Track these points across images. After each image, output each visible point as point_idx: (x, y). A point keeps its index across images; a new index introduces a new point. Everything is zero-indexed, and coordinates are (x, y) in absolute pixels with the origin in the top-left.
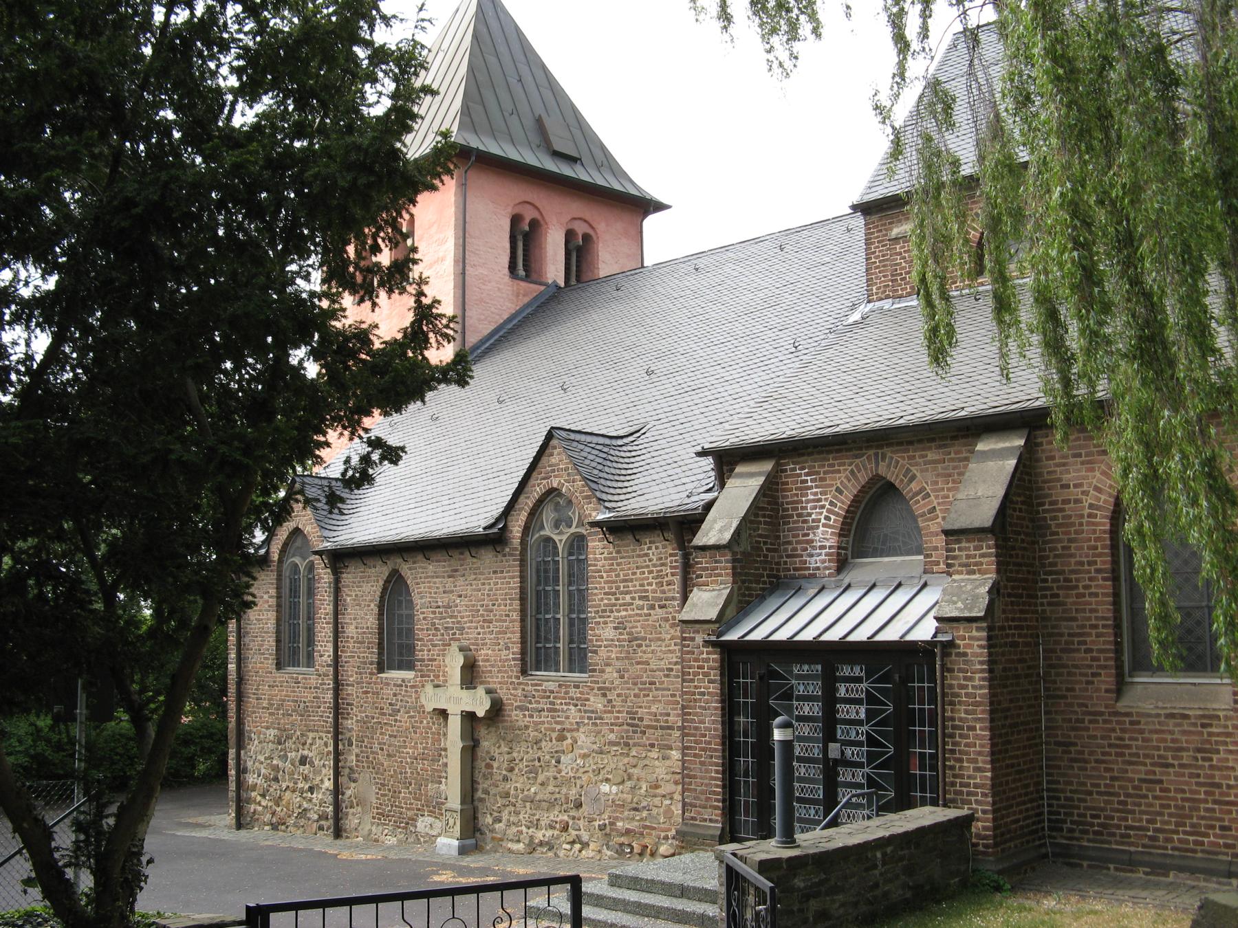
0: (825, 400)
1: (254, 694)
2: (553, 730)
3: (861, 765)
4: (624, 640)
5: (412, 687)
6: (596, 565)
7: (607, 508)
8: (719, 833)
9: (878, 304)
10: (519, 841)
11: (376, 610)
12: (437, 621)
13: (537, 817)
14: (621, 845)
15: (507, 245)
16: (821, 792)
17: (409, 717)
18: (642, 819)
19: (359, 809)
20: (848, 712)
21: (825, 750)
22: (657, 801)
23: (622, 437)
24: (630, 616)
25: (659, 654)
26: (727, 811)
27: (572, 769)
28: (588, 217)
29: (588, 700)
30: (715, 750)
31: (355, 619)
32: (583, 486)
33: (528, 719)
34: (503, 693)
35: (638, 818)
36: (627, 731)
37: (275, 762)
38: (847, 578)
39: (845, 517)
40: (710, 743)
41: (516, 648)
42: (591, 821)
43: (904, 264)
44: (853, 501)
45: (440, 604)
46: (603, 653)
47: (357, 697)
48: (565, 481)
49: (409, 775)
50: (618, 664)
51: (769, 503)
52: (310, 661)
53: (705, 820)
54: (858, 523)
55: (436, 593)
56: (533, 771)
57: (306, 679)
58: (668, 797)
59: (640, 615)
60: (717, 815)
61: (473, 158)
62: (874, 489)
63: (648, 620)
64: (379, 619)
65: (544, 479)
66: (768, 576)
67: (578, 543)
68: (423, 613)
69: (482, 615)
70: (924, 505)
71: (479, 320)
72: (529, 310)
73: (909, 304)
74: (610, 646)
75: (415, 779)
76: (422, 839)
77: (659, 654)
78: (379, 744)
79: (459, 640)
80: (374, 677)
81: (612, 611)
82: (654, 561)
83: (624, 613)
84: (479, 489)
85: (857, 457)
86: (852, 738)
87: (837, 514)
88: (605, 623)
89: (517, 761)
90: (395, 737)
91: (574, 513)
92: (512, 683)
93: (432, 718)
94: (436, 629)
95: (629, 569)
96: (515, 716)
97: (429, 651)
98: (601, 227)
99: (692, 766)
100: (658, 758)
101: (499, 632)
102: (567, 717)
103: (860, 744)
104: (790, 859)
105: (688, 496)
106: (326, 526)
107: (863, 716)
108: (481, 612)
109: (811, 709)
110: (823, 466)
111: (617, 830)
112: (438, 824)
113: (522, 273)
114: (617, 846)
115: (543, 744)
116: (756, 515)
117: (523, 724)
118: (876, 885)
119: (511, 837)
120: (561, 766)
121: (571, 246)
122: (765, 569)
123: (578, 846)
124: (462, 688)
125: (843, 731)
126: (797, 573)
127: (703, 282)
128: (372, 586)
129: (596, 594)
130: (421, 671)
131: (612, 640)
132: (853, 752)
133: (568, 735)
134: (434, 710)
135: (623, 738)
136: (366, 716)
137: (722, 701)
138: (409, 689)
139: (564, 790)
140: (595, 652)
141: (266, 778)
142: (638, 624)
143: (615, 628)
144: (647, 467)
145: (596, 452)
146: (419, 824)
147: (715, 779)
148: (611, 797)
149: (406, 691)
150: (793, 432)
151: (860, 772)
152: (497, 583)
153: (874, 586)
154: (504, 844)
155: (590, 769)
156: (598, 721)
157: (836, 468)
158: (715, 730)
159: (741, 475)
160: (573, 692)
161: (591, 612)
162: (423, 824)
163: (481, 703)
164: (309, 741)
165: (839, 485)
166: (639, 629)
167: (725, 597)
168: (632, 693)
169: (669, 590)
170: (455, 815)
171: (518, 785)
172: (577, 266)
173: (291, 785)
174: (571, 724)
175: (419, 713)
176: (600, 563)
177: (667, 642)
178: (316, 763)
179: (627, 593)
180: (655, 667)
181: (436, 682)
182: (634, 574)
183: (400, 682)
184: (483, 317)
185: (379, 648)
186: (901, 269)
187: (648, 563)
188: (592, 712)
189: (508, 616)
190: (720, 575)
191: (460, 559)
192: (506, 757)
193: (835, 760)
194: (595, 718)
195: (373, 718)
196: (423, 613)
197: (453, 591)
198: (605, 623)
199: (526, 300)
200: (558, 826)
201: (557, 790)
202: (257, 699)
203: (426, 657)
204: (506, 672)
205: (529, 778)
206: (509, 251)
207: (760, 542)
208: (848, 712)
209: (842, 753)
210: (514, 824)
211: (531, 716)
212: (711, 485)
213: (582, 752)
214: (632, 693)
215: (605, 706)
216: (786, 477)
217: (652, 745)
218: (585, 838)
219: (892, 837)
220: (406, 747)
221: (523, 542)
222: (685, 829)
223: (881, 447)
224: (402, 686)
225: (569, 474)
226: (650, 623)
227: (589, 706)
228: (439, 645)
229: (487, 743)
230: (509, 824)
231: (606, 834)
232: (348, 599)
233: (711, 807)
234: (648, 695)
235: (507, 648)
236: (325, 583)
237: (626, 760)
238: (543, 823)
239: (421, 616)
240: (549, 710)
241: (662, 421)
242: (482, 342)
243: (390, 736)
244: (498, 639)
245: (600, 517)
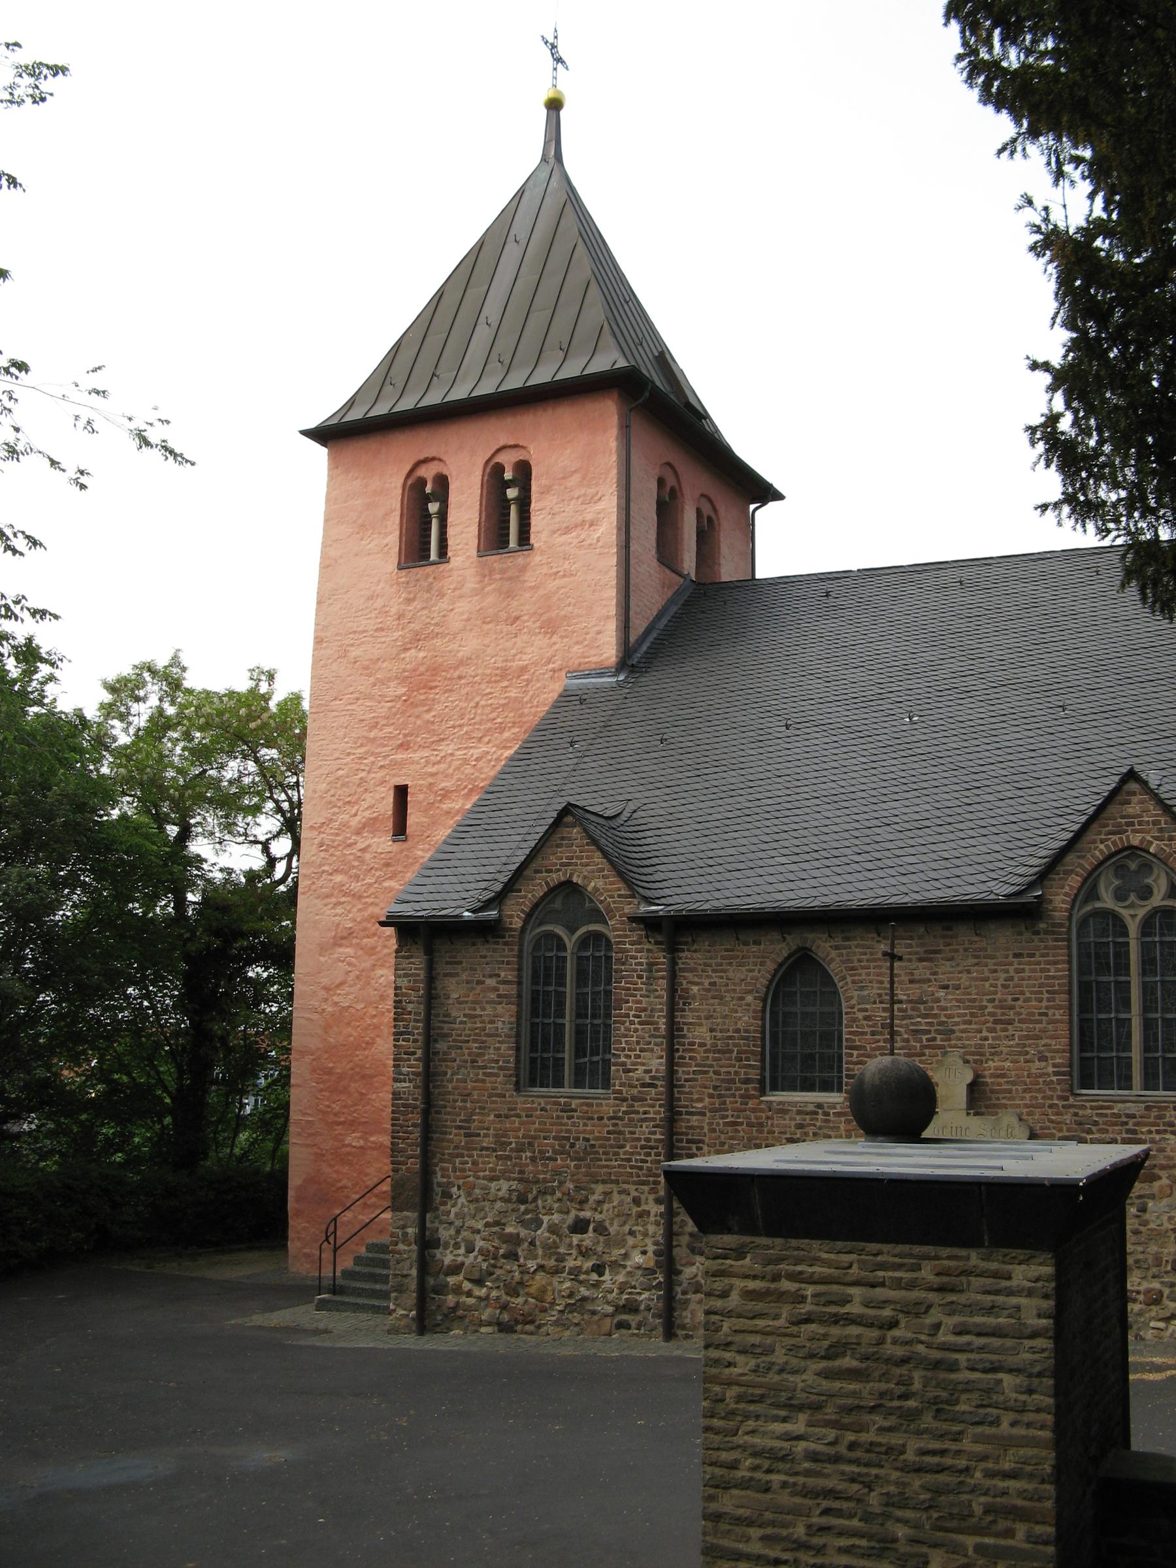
124: (968, 1114)
225: (1161, 830)
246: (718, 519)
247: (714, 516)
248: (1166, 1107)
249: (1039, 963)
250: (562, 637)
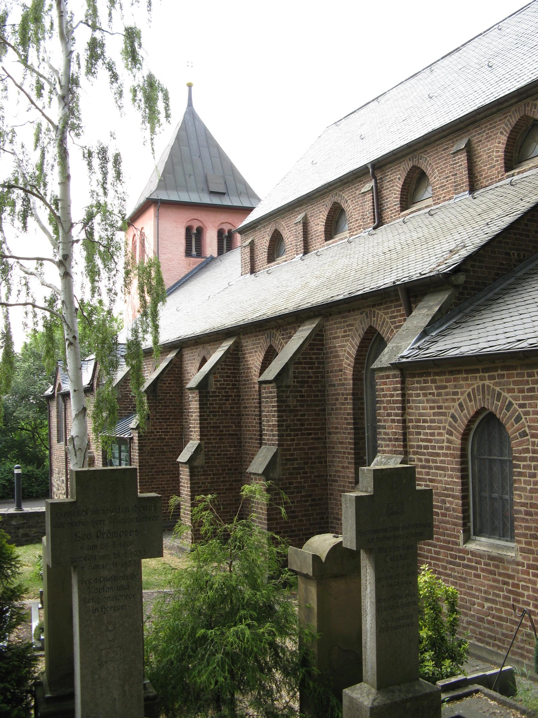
28: (230, 221)
113: (194, 253)
199: (194, 266)
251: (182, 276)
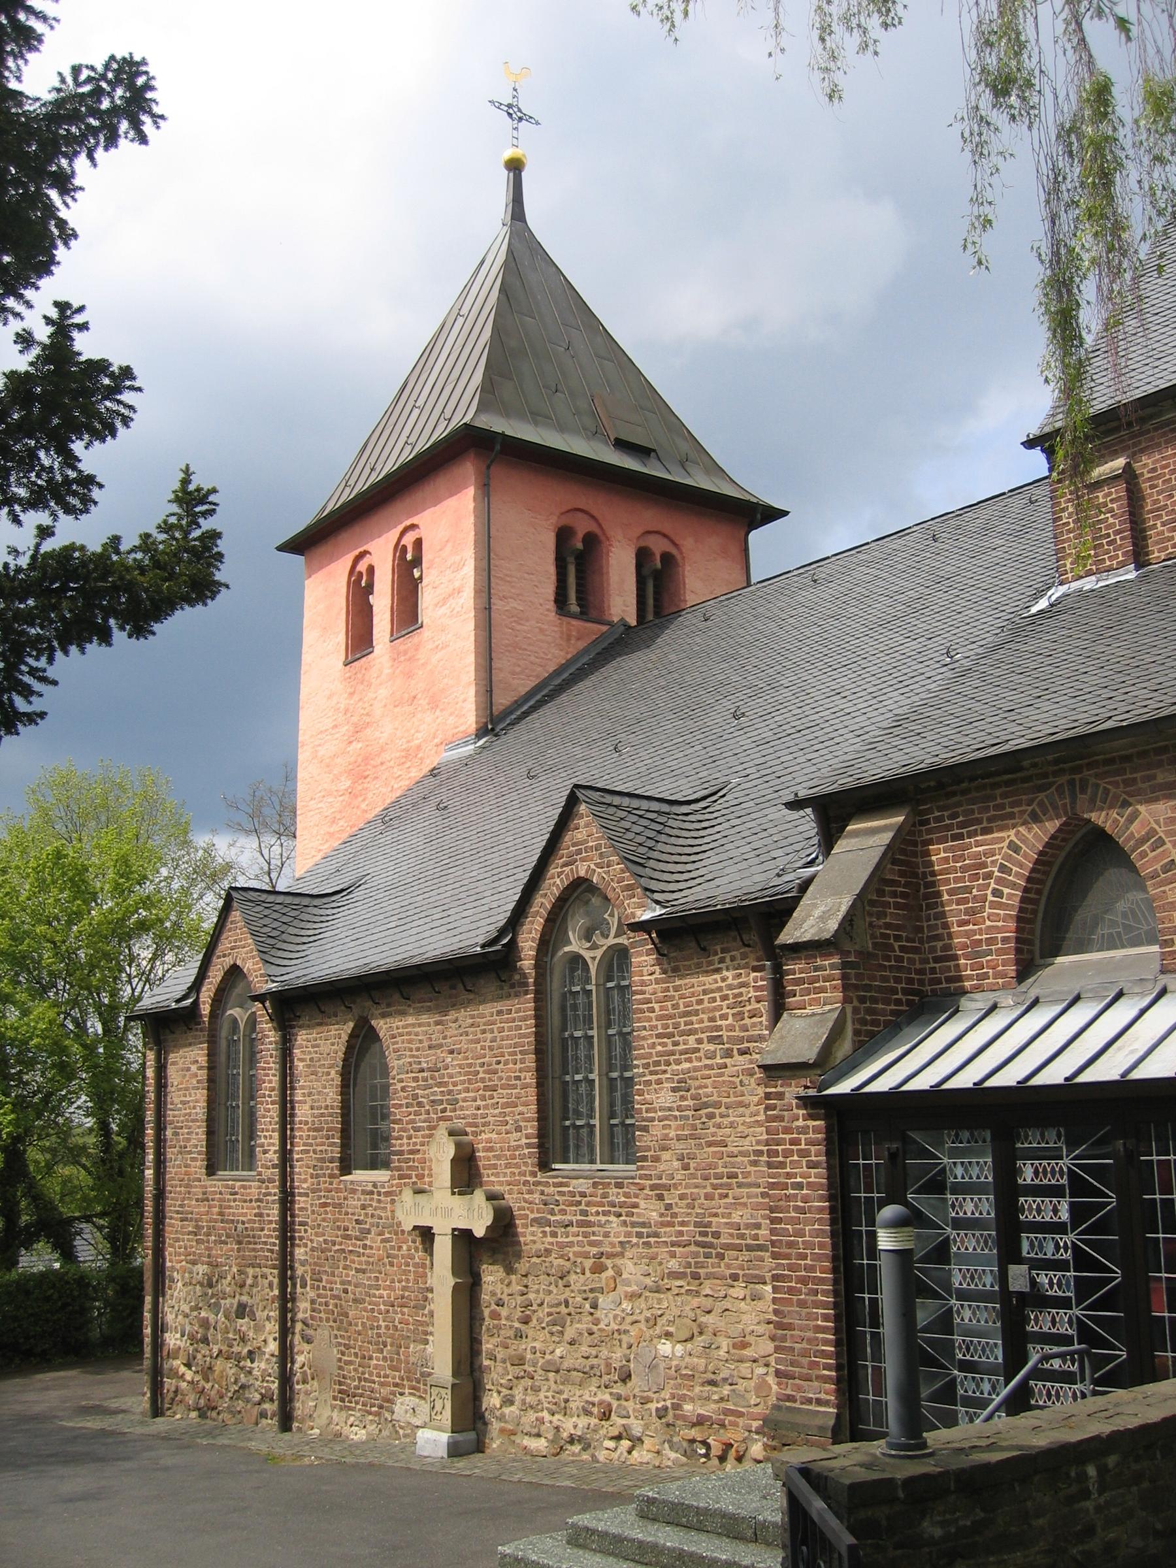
0: (988, 711)
1: (178, 1212)
2: (586, 1256)
3: (1065, 1303)
4: (688, 1108)
5: (387, 1194)
6: (643, 993)
7: (657, 902)
8: (832, 1422)
9: (1075, 585)
10: (539, 1435)
11: (338, 1080)
12: (420, 1092)
13: (565, 1396)
14: (692, 1441)
15: (552, 569)
16: (999, 1352)
17: (383, 1241)
18: (722, 1399)
19: (315, 1383)
20: (1039, 1210)
21: (1003, 1278)
22: (745, 1368)
23: (689, 803)
24: (696, 1069)
25: (741, 1128)
26: (845, 1385)
27: (615, 1317)
28: (666, 527)
29: (636, 1206)
30: (822, 1281)
31: (310, 1094)
32: (623, 871)
33: (549, 1239)
34: (512, 1200)
35: (716, 1397)
36: (696, 1255)
37: (203, 1314)
38: (1035, 986)
39: (1026, 890)
40: (811, 1268)
41: (531, 1128)
42: (645, 1401)
43: (1111, 520)
44: (1037, 862)
45: (424, 1065)
46: (656, 1130)
47: (313, 1212)
48: (597, 865)
49: (383, 1330)
50: (680, 1146)
51: (902, 874)
52: (250, 1161)
53: (809, 1401)
54: (1049, 898)
55: (418, 1049)
56: (558, 1322)
57: (244, 1187)
58: (762, 1361)
59: (710, 1067)
60: (828, 1390)
61: (498, 447)
62: (1071, 844)
63: (722, 1075)
64: (342, 1094)
65: (566, 865)
66: (906, 992)
67: (618, 959)
68: (401, 1081)
69: (483, 1080)
70: (1156, 859)
71: (513, 673)
72: (585, 660)
73: (1122, 578)
74: (666, 1118)
75: (392, 1337)
76: (401, 1432)
77: (741, 1128)
78: (342, 1283)
79: (450, 1119)
80: (336, 1181)
81: (668, 1064)
82: (730, 981)
83: (686, 1065)
84: (485, 894)
85: (1041, 789)
86: (1049, 1256)
87: (1013, 886)
88: (659, 1082)
89: (535, 1307)
90: (364, 1271)
91: (612, 915)
92: (526, 1183)
93: (414, 1242)
94: (420, 1104)
95: (693, 995)
96: (529, 1235)
97: (410, 1138)
98: (688, 543)
99: (786, 1309)
100: (744, 1299)
101: (507, 1105)
102: (606, 1235)
103: (1061, 1265)
104: (910, 1482)
105: (778, 875)
106: (272, 960)
107: (1064, 1215)
108: (481, 1075)
109: (976, 1206)
110: (987, 809)
111: (684, 1418)
112: (424, 1407)
113: (575, 608)
114: (685, 1444)
115: (572, 1278)
116: (880, 893)
117: (542, 1247)
118: (1090, 1531)
119: (527, 1429)
120: (599, 1314)
121: (646, 571)
122: (898, 980)
123: (626, 1443)
124: (453, 1193)
125: (1032, 1245)
126: (952, 985)
127: (823, 595)
128: (333, 1044)
129: (644, 1038)
130: (399, 1169)
131: (670, 1109)
132: (1051, 1280)
133: (609, 1263)
134: (415, 1228)
135: (689, 1265)
136: (325, 1241)
137: (831, 1198)
138: (382, 1198)
139: (604, 1353)
140: (645, 1129)
141: (192, 1337)
142: (708, 1081)
143: (674, 1090)
144: (724, 841)
145: (646, 823)
146: (397, 1408)
147: (824, 1330)
148: (674, 1363)
149: (379, 1201)
150: (936, 759)
151: (1063, 1315)
152: (501, 1030)
153: (1077, 999)
154: (517, 1439)
155: (641, 1318)
156: (652, 1240)
157: (1008, 810)
158: (821, 1246)
159: (856, 834)
160: (616, 1196)
161: (637, 1066)
162: (404, 1406)
163: (481, 1216)
164: (249, 1281)
165: (1013, 838)
166: (710, 1090)
167: (830, 1024)
168: (702, 1192)
169: (754, 1025)
170: (443, 1391)
171: (537, 1345)
172: (655, 600)
173: (224, 1348)
174: (613, 1245)
175: (396, 1234)
176: (649, 989)
177: (753, 1108)
178: (258, 1314)
179: (690, 1033)
180: (735, 1150)
181: (419, 1185)
182: (700, 1002)
183: (370, 1188)
184: (518, 669)
185: (342, 1138)
186: (1107, 528)
187: (720, 984)
188: (643, 1225)
189: (518, 1078)
190: (822, 990)
191: (450, 997)
192: (519, 1299)
193: (1020, 1294)
194: (647, 1233)
195: (334, 1244)
196: (401, 1081)
197: (441, 1046)
198: (659, 1082)
199: (581, 645)
200: (595, 1410)
201: (594, 1353)
202: (182, 1220)
203: (405, 1148)
204: (517, 1166)
205: (552, 1334)
206: (554, 578)
207: (887, 936)
208: (1039, 1210)
209: (1033, 1282)
210: (531, 1407)
211: (554, 1235)
212: (813, 856)
213: (629, 1289)
214: (702, 1192)
215: (662, 1215)
216: (929, 832)
217: (735, 1277)
218: (637, 1429)
219: (1116, 1436)
220: (378, 1288)
221: (539, 965)
222: (779, 1416)
223: (1078, 770)
224: (372, 1193)
225: (601, 855)
226: (726, 1078)
227: (639, 1215)
228: (422, 1128)
229: (492, 1276)
230: (526, 1407)
231: (668, 1425)
232: (301, 1064)
233: (818, 1378)
234: (726, 1196)
235: (518, 1129)
236: (271, 1043)
237: (695, 1302)
238: (572, 1405)
239: (399, 1086)
240: (581, 1224)
241: (750, 777)
242: (518, 704)
243: (357, 1271)
244: (505, 1114)
245: (647, 916)
246: (681, 553)
247: (674, 551)
248: (610, 1184)
249: (514, 1020)
250: (442, 710)
251: (551, 670)
